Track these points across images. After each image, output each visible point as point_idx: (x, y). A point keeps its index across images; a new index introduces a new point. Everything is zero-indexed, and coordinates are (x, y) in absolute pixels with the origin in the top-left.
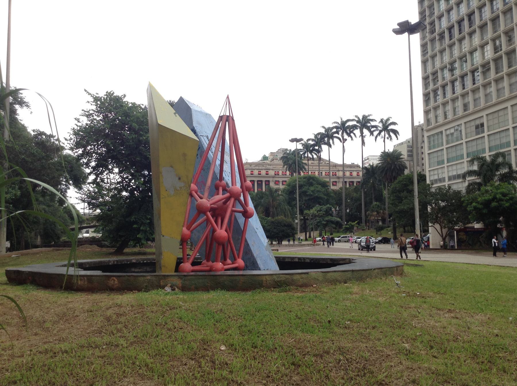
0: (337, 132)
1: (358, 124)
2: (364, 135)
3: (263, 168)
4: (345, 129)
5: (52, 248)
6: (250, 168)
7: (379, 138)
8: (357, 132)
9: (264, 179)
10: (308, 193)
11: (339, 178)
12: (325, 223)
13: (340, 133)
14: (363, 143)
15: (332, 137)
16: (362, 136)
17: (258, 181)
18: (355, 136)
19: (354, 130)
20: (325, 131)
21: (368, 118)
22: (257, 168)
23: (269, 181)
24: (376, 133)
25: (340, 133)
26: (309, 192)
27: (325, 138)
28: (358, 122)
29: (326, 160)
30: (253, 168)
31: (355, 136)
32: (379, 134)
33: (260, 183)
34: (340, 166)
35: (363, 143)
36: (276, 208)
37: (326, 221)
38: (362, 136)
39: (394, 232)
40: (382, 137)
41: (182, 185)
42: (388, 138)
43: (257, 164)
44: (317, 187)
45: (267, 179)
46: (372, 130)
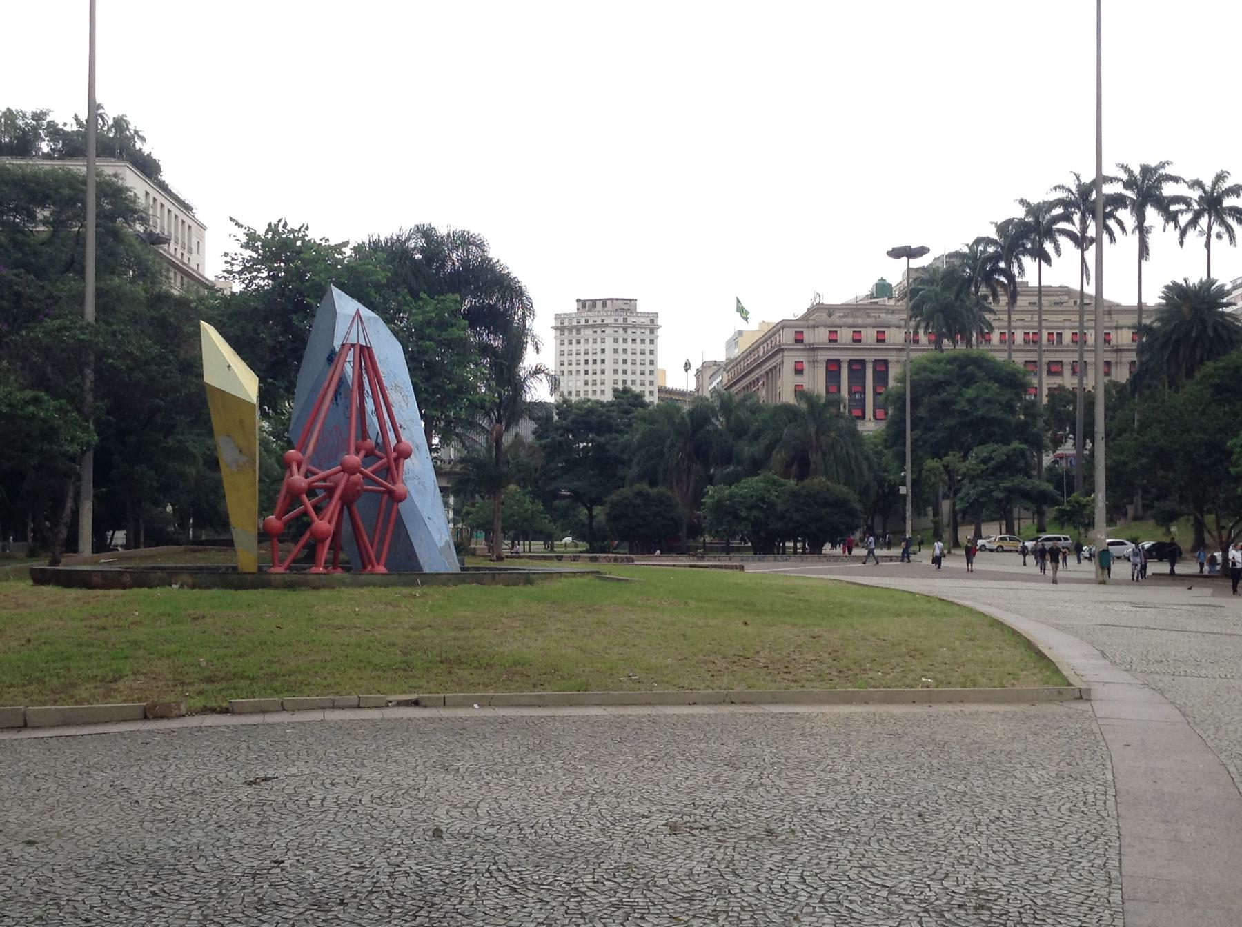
0: (1067, 218)
1: (1129, 193)
2: (1146, 224)
3: (869, 321)
4: (1090, 205)
5: (183, 547)
6: (829, 321)
7: (1191, 234)
8: (1126, 215)
9: (870, 357)
10: (957, 407)
11: (1118, 351)
12: (1001, 495)
13: (1076, 218)
14: (1144, 250)
15: (1049, 233)
16: (1142, 230)
17: (851, 362)
18: (1123, 229)
19: (1116, 209)
20: (1028, 213)
21: (1162, 171)
22: (850, 321)
23: (886, 362)
24: (1184, 219)
25: (1076, 218)
26: (962, 404)
27: (1029, 233)
28: (1127, 185)
29: (1075, 291)
30: (838, 322)
31: (1123, 229)
32: (1194, 222)
33: (857, 368)
34: (1126, 311)
35: (1144, 250)
36: (824, 454)
37: (1006, 489)
38: (1142, 230)
39: (1199, 528)
40: (1201, 233)
41: (245, 459)
42: (1219, 236)
43: (850, 310)
44: (987, 389)
45: (880, 356)
46: (1173, 208)
